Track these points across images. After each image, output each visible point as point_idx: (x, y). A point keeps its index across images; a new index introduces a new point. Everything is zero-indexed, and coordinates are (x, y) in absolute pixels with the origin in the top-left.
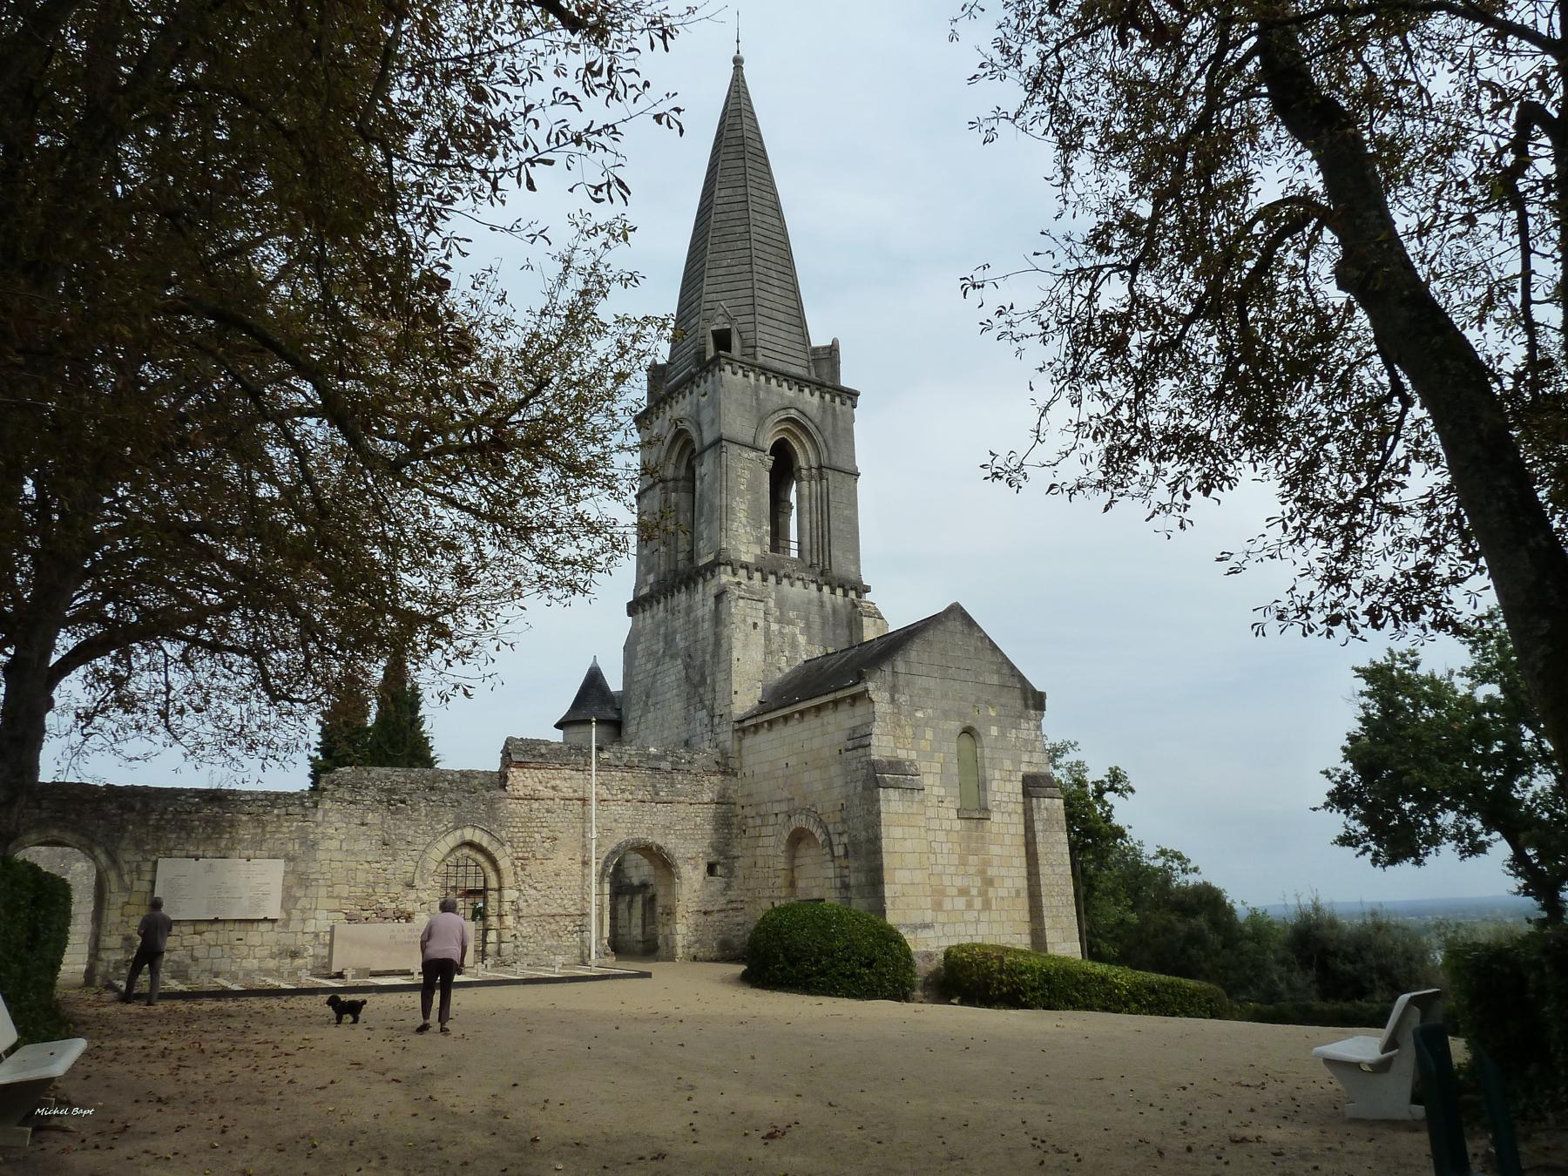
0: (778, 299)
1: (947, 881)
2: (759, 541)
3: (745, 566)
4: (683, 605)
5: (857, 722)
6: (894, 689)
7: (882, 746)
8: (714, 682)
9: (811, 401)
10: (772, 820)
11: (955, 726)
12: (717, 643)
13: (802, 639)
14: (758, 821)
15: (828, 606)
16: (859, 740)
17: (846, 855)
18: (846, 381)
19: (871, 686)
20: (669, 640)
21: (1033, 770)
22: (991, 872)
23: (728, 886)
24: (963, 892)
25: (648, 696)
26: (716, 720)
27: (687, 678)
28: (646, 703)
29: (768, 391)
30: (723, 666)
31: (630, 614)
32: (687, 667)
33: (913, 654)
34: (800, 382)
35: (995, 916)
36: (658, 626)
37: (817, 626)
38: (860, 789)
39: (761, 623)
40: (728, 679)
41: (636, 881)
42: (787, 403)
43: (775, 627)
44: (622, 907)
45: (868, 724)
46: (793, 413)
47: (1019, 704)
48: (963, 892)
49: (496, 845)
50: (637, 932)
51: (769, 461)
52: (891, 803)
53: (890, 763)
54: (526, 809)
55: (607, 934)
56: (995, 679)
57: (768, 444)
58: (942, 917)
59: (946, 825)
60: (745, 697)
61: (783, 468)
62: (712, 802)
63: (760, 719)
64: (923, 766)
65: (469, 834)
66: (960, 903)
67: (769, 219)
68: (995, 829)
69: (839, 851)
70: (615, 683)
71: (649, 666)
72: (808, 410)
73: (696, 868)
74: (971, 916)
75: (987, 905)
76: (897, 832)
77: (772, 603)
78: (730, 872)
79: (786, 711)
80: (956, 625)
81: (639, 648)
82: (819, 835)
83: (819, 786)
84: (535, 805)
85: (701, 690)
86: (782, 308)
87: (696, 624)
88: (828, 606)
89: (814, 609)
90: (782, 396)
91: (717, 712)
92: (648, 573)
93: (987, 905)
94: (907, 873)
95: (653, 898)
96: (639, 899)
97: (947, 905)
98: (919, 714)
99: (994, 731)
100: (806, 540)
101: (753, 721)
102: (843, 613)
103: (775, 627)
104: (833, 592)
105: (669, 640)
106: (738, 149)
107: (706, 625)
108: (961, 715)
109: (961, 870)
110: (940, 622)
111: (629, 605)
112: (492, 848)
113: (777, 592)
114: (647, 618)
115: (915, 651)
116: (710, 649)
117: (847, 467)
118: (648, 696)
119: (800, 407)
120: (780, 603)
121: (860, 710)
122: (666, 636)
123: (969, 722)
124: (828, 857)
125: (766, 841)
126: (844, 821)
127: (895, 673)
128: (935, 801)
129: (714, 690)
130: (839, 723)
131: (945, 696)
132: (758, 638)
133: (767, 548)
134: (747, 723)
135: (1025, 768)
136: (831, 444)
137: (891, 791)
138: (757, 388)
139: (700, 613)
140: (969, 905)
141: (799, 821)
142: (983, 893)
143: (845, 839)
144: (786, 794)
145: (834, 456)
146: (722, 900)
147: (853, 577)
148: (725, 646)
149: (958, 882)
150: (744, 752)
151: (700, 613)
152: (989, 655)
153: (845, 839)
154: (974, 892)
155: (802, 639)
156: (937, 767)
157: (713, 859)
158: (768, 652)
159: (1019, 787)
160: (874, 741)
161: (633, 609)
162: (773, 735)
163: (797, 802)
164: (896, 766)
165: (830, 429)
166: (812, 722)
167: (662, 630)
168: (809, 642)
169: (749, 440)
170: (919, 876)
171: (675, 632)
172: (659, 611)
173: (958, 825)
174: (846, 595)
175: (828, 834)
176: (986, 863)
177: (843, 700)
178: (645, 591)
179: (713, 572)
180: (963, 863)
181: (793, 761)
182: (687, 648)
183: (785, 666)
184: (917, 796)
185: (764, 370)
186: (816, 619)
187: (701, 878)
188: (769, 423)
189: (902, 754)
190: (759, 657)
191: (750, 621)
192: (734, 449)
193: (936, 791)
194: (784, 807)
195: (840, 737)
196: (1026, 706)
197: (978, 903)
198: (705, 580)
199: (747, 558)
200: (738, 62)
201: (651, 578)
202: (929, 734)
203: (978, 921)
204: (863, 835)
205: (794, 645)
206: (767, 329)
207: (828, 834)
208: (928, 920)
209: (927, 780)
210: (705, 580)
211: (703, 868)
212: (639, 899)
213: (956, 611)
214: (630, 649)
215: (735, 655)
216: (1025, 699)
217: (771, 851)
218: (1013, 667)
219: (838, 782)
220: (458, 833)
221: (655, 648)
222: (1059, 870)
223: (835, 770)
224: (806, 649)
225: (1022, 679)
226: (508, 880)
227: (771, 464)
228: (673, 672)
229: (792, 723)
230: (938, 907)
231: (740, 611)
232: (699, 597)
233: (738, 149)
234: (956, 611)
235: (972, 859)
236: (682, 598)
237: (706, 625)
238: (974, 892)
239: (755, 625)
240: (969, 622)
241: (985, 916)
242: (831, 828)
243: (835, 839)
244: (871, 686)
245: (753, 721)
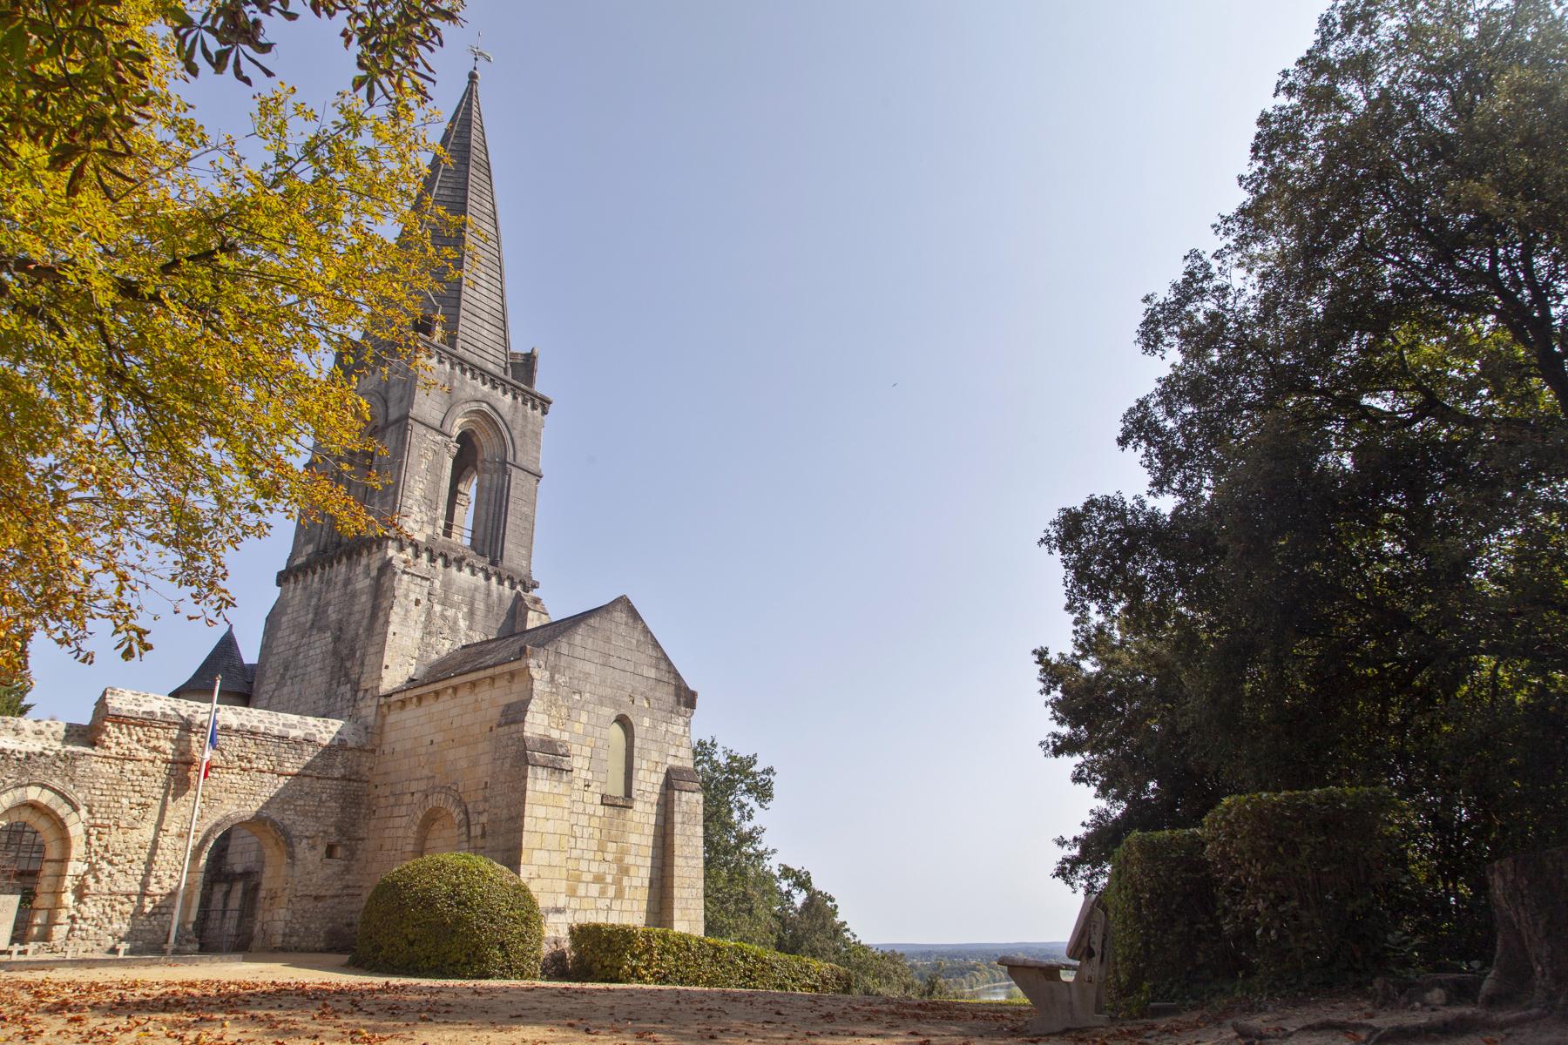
0: (484, 300)
1: (583, 866)
2: (433, 522)
3: (415, 545)
4: (341, 577)
5: (513, 699)
6: (554, 670)
7: (536, 724)
8: (364, 655)
9: (505, 401)
10: (407, 798)
11: (610, 713)
12: (374, 617)
13: (463, 624)
14: (392, 800)
15: (495, 595)
16: (515, 714)
17: (483, 835)
18: (539, 387)
19: (532, 662)
20: (320, 612)
21: (677, 763)
22: (629, 860)
23: (347, 870)
24: (599, 879)
25: (286, 669)
26: (361, 694)
27: (335, 653)
28: (283, 677)
29: (463, 382)
30: (377, 639)
31: (279, 584)
32: (337, 639)
33: (578, 639)
34: (494, 381)
35: (626, 905)
36: (310, 597)
37: (480, 614)
38: (507, 765)
39: (424, 602)
40: (381, 653)
41: (239, 869)
42: (479, 396)
43: (438, 608)
44: (218, 895)
45: (526, 703)
46: (485, 407)
47: (672, 699)
48: (599, 879)
49: (68, 808)
50: (231, 925)
51: (454, 448)
52: (539, 784)
53: (542, 741)
54: (116, 770)
55: (193, 917)
56: (652, 673)
57: (456, 432)
58: (574, 903)
59: (590, 810)
60: (396, 670)
61: (467, 458)
62: (343, 778)
63: (409, 694)
64: (575, 749)
65: (33, 794)
66: (595, 889)
67: (486, 227)
68: (636, 818)
69: (476, 830)
70: (250, 654)
71: (293, 638)
72: (499, 406)
73: (313, 847)
74: (602, 903)
75: (619, 895)
76: (540, 811)
77: (437, 584)
78: (352, 854)
79: (439, 686)
80: (620, 616)
81: (284, 619)
82: (457, 815)
83: (463, 764)
84: (129, 766)
85: (348, 664)
86: (487, 309)
87: (354, 595)
88: (495, 595)
89: (480, 596)
90: (476, 389)
91: (363, 685)
92: (308, 542)
93: (619, 895)
94: (544, 854)
95: (256, 888)
96: (239, 888)
97: (581, 890)
98: (577, 697)
99: (647, 722)
100: (481, 529)
101: (401, 696)
102: (508, 604)
103: (438, 608)
104: (501, 582)
105: (320, 612)
106: (462, 133)
107: (364, 598)
108: (616, 703)
109: (599, 856)
110: (608, 612)
111: (280, 574)
112: (63, 810)
113: (445, 575)
114: (296, 591)
115: (579, 635)
116: (365, 622)
117: (532, 468)
118: (286, 669)
119: (492, 402)
120: (447, 585)
121: (517, 686)
122: (317, 607)
123: (623, 711)
124: (464, 837)
125: (397, 822)
126: (486, 800)
127: (558, 654)
128: (581, 784)
129: (362, 664)
130: (493, 698)
131: (603, 682)
132: (417, 614)
133: (440, 531)
134: (394, 698)
135: (671, 761)
136: (518, 442)
137: (539, 770)
138: (451, 378)
139: (359, 586)
140: (603, 893)
141: (435, 801)
142: (618, 882)
143: (484, 819)
144: (426, 772)
145: (519, 455)
146: (338, 885)
147: (524, 572)
148: (381, 620)
149: (594, 867)
150: (387, 728)
151: (359, 586)
152: (650, 651)
153: (484, 819)
154: (609, 879)
155: (463, 624)
156: (587, 751)
157: (333, 839)
158: (428, 631)
159: (662, 778)
160: (529, 718)
161: (282, 578)
162: (421, 711)
163: (437, 781)
164: (548, 745)
165: (519, 428)
166: (465, 697)
167: (314, 601)
168: (470, 628)
169: (437, 424)
170: (557, 859)
171: (328, 604)
172: (315, 581)
173: (600, 810)
174: (512, 587)
175: (466, 813)
176: (623, 853)
177: (501, 675)
178: (300, 561)
179: (379, 547)
180: (602, 849)
181: (438, 738)
182: (340, 621)
183: (445, 646)
184: (565, 777)
185: (462, 361)
186: (480, 606)
187: (318, 859)
188: (461, 410)
189: (555, 734)
190: (418, 634)
191: (413, 597)
192: (419, 429)
193: (584, 774)
194: (423, 785)
195: (494, 714)
196: (678, 703)
197: (611, 891)
198: (370, 553)
199: (420, 537)
200: (473, 77)
201: (310, 548)
202: (584, 717)
203: (609, 909)
204: (504, 814)
205: (454, 629)
206: (469, 324)
207: (466, 813)
208: (560, 904)
209: (577, 763)
210: (370, 553)
211: (322, 849)
212: (239, 888)
213: (623, 603)
214: (273, 621)
215: (391, 629)
216: (678, 696)
217: (401, 833)
218: (670, 664)
219: (486, 759)
220: (20, 790)
221: (302, 619)
222: (692, 863)
223: (483, 746)
224: (465, 631)
225: (677, 676)
226: (78, 849)
227: (455, 451)
228: (322, 643)
229: (444, 698)
230: (572, 893)
231: (407, 589)
232: (360, 570)
233: (462, 133)
234: (623, 603)
235: (612, 847)
236: (342, 569)
237: (364, 598)
238: (609, 879)
239: (417, 602)
240: (634, 614)
241: (616, 905)
242: (470, 807)
243: (473, 818)
244: (532, 662)
245: (401, 696)
